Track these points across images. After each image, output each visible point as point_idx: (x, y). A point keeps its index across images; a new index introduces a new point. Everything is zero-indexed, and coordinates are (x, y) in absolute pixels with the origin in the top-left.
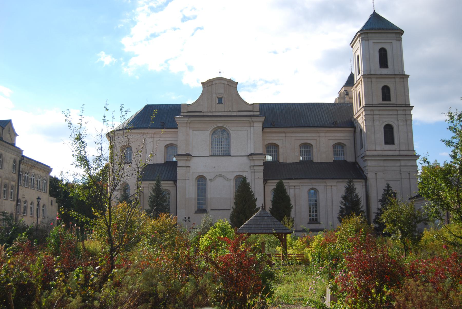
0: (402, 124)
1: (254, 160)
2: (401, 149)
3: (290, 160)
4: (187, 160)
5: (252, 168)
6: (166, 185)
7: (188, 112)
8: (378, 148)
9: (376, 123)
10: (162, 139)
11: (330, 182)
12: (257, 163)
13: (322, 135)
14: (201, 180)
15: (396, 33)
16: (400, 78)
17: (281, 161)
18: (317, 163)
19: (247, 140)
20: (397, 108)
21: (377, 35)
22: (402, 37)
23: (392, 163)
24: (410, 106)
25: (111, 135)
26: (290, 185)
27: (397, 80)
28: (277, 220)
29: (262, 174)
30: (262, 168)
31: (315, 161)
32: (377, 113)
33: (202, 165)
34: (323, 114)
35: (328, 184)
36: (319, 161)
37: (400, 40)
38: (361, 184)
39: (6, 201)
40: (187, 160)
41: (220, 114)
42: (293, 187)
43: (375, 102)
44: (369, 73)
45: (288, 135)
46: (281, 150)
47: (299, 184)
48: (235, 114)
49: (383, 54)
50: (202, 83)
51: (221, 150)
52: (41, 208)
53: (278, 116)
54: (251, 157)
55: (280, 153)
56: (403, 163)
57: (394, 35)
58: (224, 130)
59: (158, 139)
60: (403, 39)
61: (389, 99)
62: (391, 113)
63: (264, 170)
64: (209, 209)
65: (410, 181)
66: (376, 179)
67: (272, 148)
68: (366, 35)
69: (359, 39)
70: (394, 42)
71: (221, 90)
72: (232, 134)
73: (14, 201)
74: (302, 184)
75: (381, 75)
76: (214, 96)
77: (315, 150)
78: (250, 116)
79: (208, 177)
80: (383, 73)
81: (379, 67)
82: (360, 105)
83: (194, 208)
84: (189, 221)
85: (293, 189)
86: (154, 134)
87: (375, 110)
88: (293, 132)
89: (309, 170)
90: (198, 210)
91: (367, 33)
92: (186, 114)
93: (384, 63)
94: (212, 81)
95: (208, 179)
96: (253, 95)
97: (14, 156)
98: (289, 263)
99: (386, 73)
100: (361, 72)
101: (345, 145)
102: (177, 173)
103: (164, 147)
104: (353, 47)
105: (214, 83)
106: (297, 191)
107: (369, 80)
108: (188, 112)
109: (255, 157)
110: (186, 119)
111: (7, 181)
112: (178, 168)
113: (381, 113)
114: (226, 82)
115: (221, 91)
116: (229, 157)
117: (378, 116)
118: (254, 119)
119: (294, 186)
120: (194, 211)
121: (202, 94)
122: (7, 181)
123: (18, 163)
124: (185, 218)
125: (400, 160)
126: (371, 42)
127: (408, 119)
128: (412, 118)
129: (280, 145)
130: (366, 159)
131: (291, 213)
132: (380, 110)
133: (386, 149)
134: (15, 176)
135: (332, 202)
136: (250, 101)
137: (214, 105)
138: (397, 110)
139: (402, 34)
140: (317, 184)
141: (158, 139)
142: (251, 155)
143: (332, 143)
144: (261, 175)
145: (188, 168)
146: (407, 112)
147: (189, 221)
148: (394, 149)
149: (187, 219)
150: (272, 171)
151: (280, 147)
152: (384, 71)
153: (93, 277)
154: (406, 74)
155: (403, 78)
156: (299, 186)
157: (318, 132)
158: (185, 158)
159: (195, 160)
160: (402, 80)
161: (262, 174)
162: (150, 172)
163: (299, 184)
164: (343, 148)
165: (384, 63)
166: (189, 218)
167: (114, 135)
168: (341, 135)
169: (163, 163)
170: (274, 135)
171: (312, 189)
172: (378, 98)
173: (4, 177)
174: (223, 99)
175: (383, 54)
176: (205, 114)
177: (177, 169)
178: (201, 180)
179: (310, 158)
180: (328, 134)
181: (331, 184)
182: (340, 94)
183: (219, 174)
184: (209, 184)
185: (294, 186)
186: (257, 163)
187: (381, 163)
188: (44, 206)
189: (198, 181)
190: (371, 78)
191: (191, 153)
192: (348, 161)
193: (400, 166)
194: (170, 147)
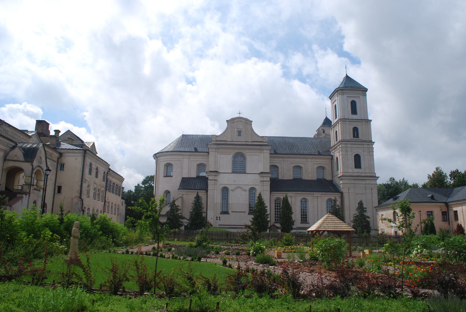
1: (263, 177)
2: (366, 172)
5: (262, 182)
6: (202, 194)
7: (253, 142)
9: (349, 153)
10: (195, 160)
11: (316, 194)
13: (309, 160)
15: (363, 91)
17: (280, 178)
18: (305, 180)
19: (258, 163)
21: (350, 91)
22: (367, 93)
25: (157, 155)
26: (315, 195)
27: (347, 122)
28: (341, 221)
29: (269, 187)
32: (350, 146)
33: (227, 179)
35: (315, 195)
36: (307, 179)
37: (366, 95)
39: (99, 202)
43: (348, 138)
45: (285, 159)
46: (280, 170)
47: (320, 195)
48: (250, 143)
49: (353, 104)
51: (239, 167)
52: (117, 207)
53: (279, 147)
56: (367, 182)
57: (361, 92)
58: (242, 156)
59: (192, 160)
61: (358, 136)
62: (359, 146)
67: (274, 167)
68: (342, 91)
70: (361, 97)
71: (240, 125)
72: (248, 158)
73: (102, 201)
76: (236, 130)
77: (304, 171)
78: (261, 145)
79: (230, 188)
80: (354, 118)
82: (337, 140)
83: (219, 211)
86: (190, 155)
88: (289, 158)
89: (298, 184)
90: (222, 212)
91: (343, 90)
92: (215, 142)
93: (354, 111)
96: (263, 130)
97: (104, 169)
99: (356, 118)
100: (337, 117)
101: (325, 168)
105: (235, 121)
106: (293, 199)
107: (344, 123)
108: (253, 142)
109: (264, 175)
110: (215, 146)
111: (100, 187)
112: (208, 181)
113: (352, 146)
114: (244, 121)
115: (241, 127)
118: (264, 147)
121: (227, 129)
122: (100, 187)
123: (106, 174)
126: (345, 96)
127: (371, 151)
131: (293, 216)
132: (351, 144)
134: (104, 183)
139: (366, 91)
141: (192, 160)
142: (261, 173)
143: (316, 166)
144: (268, 188)
145: (216, 182)
146: (370, 146)
149: (218, 218)
150: (276, 184)
152: (354, 117)
153: (395, 257)
158: (214, 174)
160: (367, 123)
162: (186, 183)
163: (320, 195)
165: (354, 111)
167: (157, 155)
170: (276, 159)
171: (304, 199)
172: (350, 136)
173: (98, 184)
174: (242, 132)
175: (353, 104)
178: (225, 190)
180: (313, 160)
182: (318, 130)
184: (230, 193)
187: (352, 182)
188: (118, 205)
189: (223, 191)
194: (201, 166)
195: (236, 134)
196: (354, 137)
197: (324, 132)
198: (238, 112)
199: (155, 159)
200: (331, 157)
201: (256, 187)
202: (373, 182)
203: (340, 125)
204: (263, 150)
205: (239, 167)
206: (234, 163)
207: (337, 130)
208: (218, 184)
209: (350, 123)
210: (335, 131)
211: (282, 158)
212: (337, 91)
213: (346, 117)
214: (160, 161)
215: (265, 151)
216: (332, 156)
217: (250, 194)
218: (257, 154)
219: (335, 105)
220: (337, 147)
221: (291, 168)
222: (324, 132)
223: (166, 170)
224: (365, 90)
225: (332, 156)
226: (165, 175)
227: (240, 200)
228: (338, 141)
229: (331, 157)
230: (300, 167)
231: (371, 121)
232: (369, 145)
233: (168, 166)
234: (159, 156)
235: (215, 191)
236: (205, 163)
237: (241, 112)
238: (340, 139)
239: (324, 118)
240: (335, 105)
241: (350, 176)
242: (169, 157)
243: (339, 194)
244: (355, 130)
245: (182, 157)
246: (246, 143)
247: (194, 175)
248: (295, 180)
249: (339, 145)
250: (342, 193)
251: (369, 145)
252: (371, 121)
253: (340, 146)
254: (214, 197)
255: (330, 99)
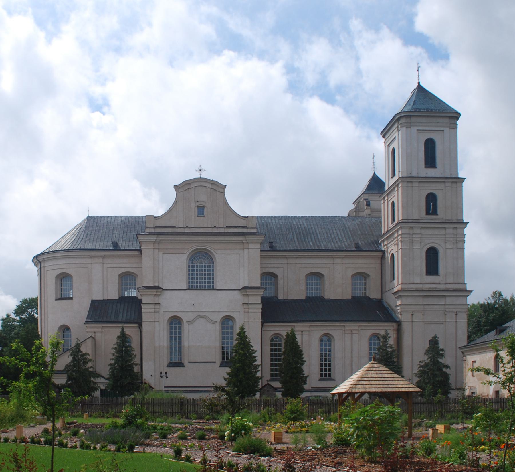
0: (450, 247)
1: (248, 295)
2: (448, 281)
3: (293, 296)
4: (155, 295)
5: (246, 306)
6: (131, 330)
8: (417, 280)
9: (417, 246)
10: (115, 266)
12: (252, 299)
13: (338, 261)
14: (175, 323)
16: (408, 182)
17: (280, 297)
18: (330, 300)
19: (238, 268)
20: (446, 225)
21: (424, 120)
22: (458, 122)
23: (435, 301)
24: (463, 223)
25: (41, 258)
26: (347, 328)
30: (260, 306)
31: (326, 298)
33: (177, 301)
34: (339, 233)
35: (347, 328)
36: (332, 298)
37: (455, 127)
38: (392, 328)
40: (155, 295)
41: (201, 231)
42: (300, 333)
43: (416, 217)
44: (410, 175)
46: (280, 282)
47: (308, 329)
48: (222, 231)
49: (430, 146)
50: (175, 186)
51: (201, 278)
53: (279, 237)
54: (244, 291)
55: (279, 286)
56: (449, 301)
57: (447, 120)
59: (109, 266)
60: (458, 126)
61: (435, 212)
62: (437, 231)
63: (262, 309)
64: (185, 362)
65: (456, 324)
66: (456, 322)
68: (408, 120)
69: (396, 125)
70: (447, 130)
74: (313, 329)
75: (426, 177)
76: (193, 205)
77: (327, 282)
79: (185, 318)
80: (429, 175)
81: (424, 166)
82: (393, 220)
83: (165, 361)
84: (167, 377)
85: (300, 336)
86: (104, 257)
87: (449, 228)
90: (171, 363)
91: (410, 116)
92: (152, 230)
93: (430, 160)
94: (190, 184)
95: (184, 321)
96: (249, 202)
98: (479, 422)
99: (433, 175)
100: (397, 173)
101: (368, 276)
102: (142, 313)
103: (117, 277)
104: (386, 137)
105: (192, 186)
109: (249, 292)
110: (154, 238)
113: (423, 231)
114: (209, 185)
115: (203, 197)
116: (214, 291)
117: (419, 236)
118: (249, 238)
119: (95, 332)
120: (166, 364)
121: (176, 202)
124: (161, 373)
125: (445, 296)
126: (414, 129)
127: (459, 241)
128: (465, 239)
129: (280, 276)
130: (400, 294)
132: (422, 228)
133: (428, 281)
135: (352, 352)
136: (242, 213)
137: (193, 217)
138: (445, 228)
140: (332, 328)
141: (109, 266)
142: (245, 288)
143: (350, 273)
145: (157, 306)
146: (459, 231)
147: (167, 377)
148: (437, 282)
149: (163, 374)
150: (273, 310)
151: (279, 278)
152: (431, 172)
154: (460, 176)
155: (456, 182)
156: (309, 331)
157: (333, 257)
158: (154, 292)
159: (167, 295)
160: (454, 185)
161: (259, 315)
163: (357, 328)
164: (365, 280)
165: (430, 160)
166: (166, 373)
168: (365, 264)
169: (117, 298)
170: (272, 261)
171: (326, 335)
172: (419, 211)
175: (430, 146)
176: (180, 231)
177: (142, 307)
178: (175, 323)
179: (365, 293)
181: (352, 329)
183: (201, 313)
184: (186, 327)
185: (302, 332)
186: (252, 299)
187: (420, 301)
190: (412, 182)
191: (160, 286)
192: (371, 297)
193: (445, 304)
195: (194, 212)
196: (428, 213)
197: (368, 205)
198: (198, 168)
199: (36, 265)
200: (380, 254)
201: (235, 315)
202: (460, 301)
203: (400, 189)
204: (248, 243)
205: (201, 278)
206: (191, 270)
207: (395, 200)
208: (161, 311)
209: (422, 185)
210: (390, 202)
211: (286, 257)
212: (398, 120)
213: (414, 174)
214: (46, 269)
215: (251, 246)
216: (384, 252)
217: (223, 328)
218: (236, 251)
219: (393, 150)
220: (393, 234)
221: (303, 277)
222: (368, 205)
223: (59, 287)
224: (456, 116)
225: (384, 252)
226: (59, 297)
227: (204, 341)
228: (396, 221)
229: (380, 254)
230: (319, 276)
231: (463, 179)
232: (456, 228)
233: (63, 278)
234: (45, 260)
235: (157, 324)
236: (134, 271)
237: (203, 168)
238: (400, 218)
239: (370, 176)
240: (393, 150)
241: (417, 290)
242: (63, 261)
243: (394, 324)
244: (431, 200)
245: (89, 261)
246: (215, 230)
247: (114, 295)
248: (309, 299)
249: (397, 231)
250: (399, 323)
251: (456, 228)
252: (463, 179)
253: (400, 232)
254: (154, 335)
255: (384, 137)
